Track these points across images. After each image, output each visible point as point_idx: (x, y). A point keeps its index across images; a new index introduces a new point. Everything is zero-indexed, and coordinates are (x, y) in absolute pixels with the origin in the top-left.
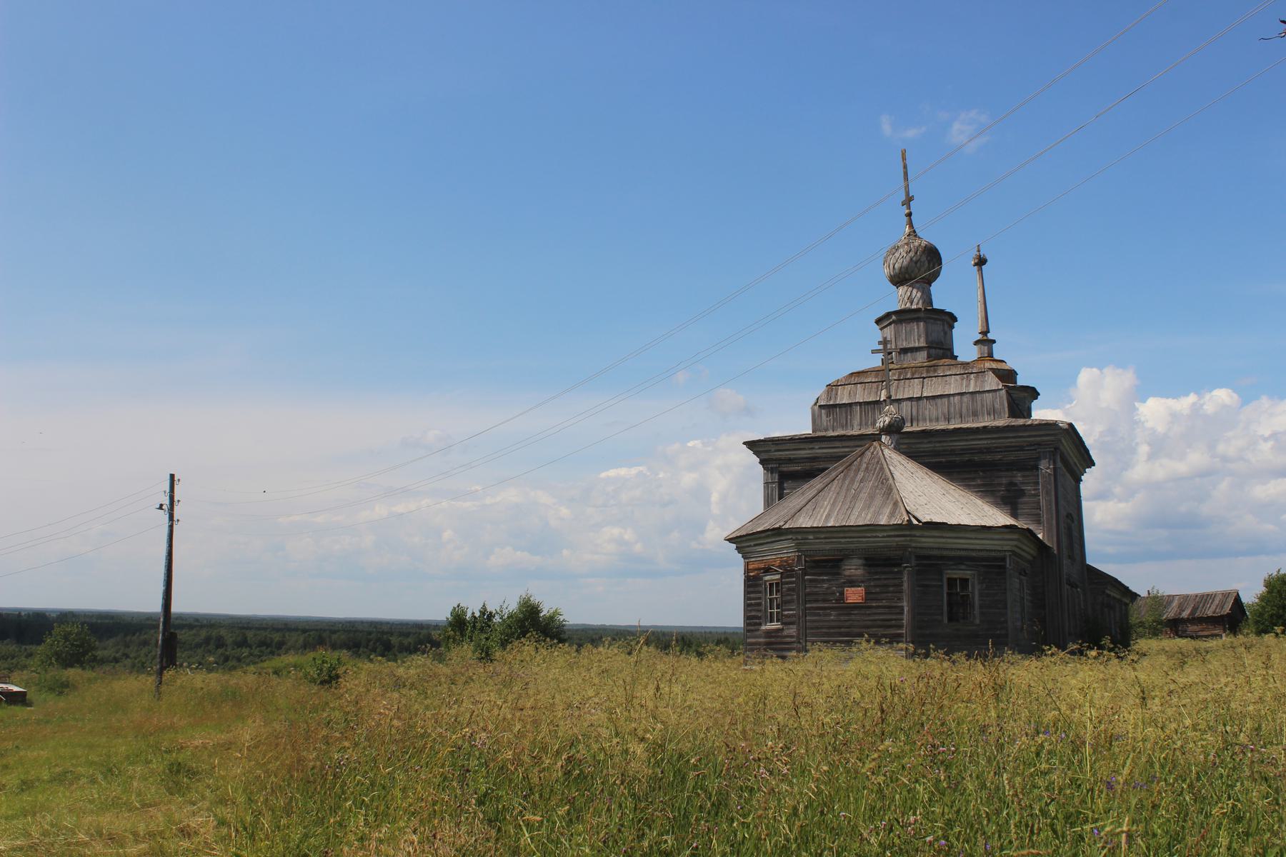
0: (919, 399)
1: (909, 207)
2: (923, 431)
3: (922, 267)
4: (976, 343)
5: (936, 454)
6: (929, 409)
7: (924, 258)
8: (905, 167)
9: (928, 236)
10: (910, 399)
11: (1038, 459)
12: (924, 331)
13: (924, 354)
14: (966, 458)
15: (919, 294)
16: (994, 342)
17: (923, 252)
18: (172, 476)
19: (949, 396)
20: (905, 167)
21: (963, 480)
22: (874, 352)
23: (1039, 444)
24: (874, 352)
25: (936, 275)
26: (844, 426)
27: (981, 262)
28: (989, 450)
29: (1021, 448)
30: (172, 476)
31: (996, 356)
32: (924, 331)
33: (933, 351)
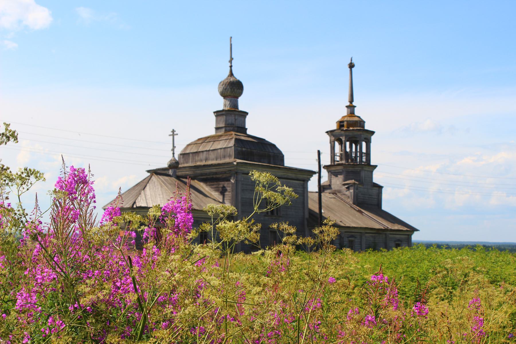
0: (209, 150)
1: (231, 63)
2: (195, 166)
3: (233, 89)
4: (347, 107)
5: (202, 175)
6: (212, 155)
7: (228, 87)
8: (231, 45)
9: (238, 76)
10: (206, 151)
11: (231, 177)
12: (232, 119)
13: (224, 130)
14: (211, 176)
15: (229, 103)
16: (355, 107)
17: (228, 84)
18: (319, 152)
19: (217, 149)
20: (231, 45)
21: (210, 185)
22: (177, 134)
23: (230, 171)
24: (177, 134)
25: (240, 94)
26: (187, 163)
27: (351, 66)
28: (216, 173)
29: (225, 173)
30: (319, 152)
31: (356, 113)
32: (232, 119)
33: (228, 128)
